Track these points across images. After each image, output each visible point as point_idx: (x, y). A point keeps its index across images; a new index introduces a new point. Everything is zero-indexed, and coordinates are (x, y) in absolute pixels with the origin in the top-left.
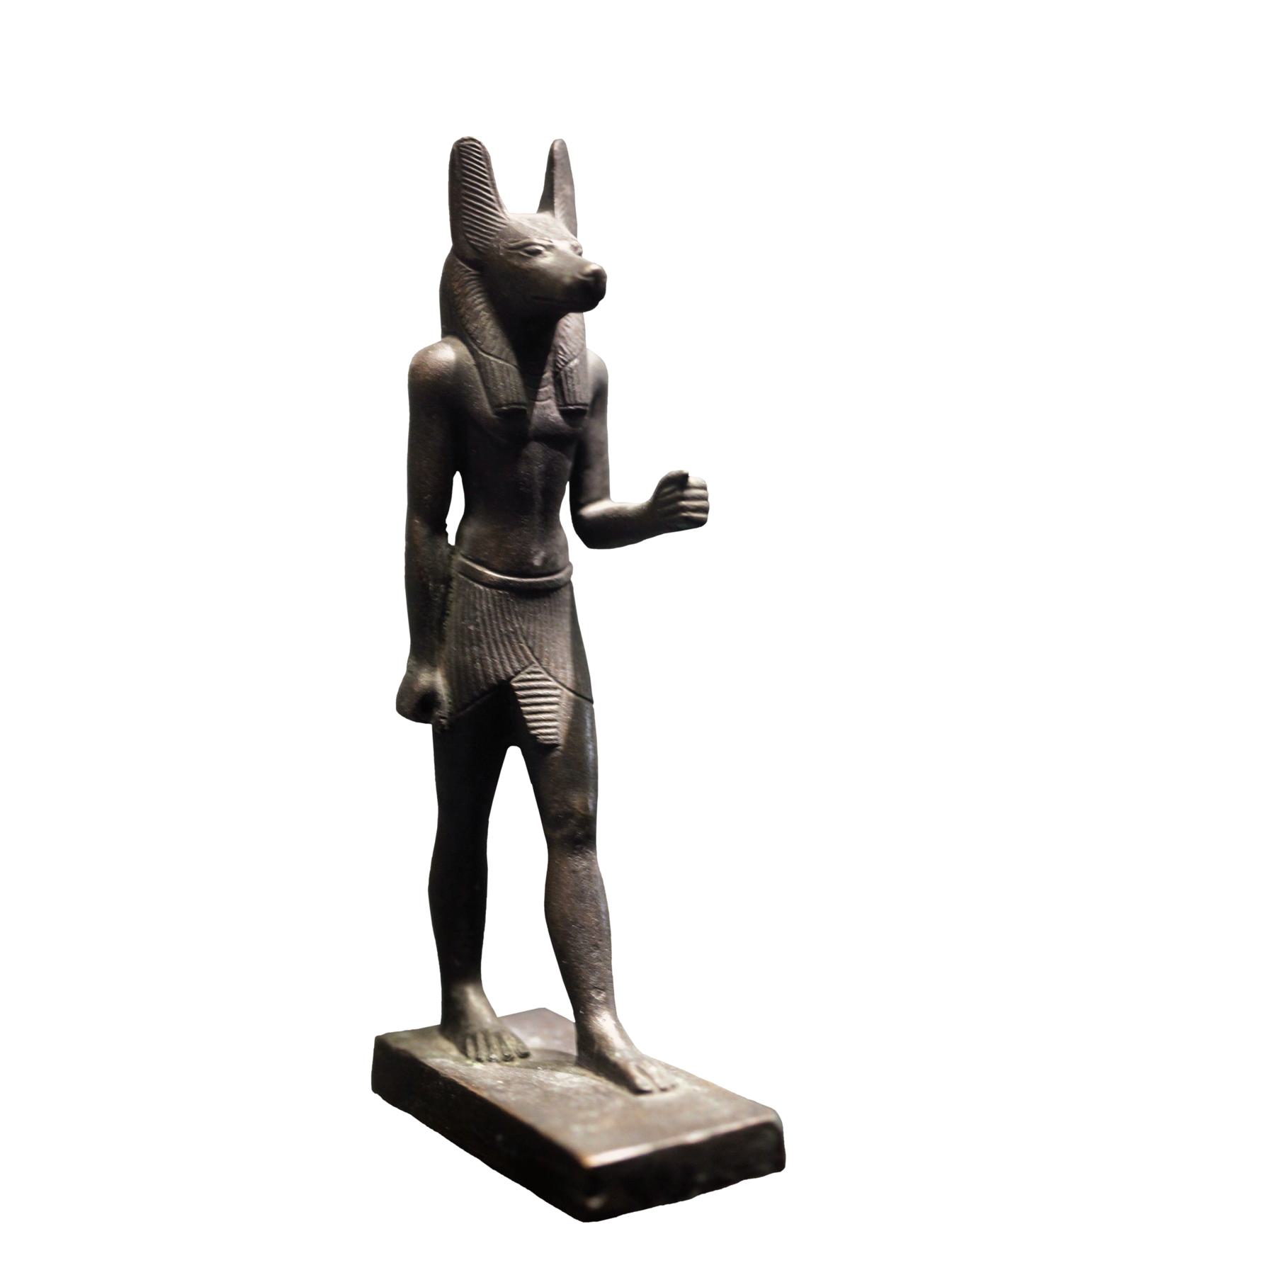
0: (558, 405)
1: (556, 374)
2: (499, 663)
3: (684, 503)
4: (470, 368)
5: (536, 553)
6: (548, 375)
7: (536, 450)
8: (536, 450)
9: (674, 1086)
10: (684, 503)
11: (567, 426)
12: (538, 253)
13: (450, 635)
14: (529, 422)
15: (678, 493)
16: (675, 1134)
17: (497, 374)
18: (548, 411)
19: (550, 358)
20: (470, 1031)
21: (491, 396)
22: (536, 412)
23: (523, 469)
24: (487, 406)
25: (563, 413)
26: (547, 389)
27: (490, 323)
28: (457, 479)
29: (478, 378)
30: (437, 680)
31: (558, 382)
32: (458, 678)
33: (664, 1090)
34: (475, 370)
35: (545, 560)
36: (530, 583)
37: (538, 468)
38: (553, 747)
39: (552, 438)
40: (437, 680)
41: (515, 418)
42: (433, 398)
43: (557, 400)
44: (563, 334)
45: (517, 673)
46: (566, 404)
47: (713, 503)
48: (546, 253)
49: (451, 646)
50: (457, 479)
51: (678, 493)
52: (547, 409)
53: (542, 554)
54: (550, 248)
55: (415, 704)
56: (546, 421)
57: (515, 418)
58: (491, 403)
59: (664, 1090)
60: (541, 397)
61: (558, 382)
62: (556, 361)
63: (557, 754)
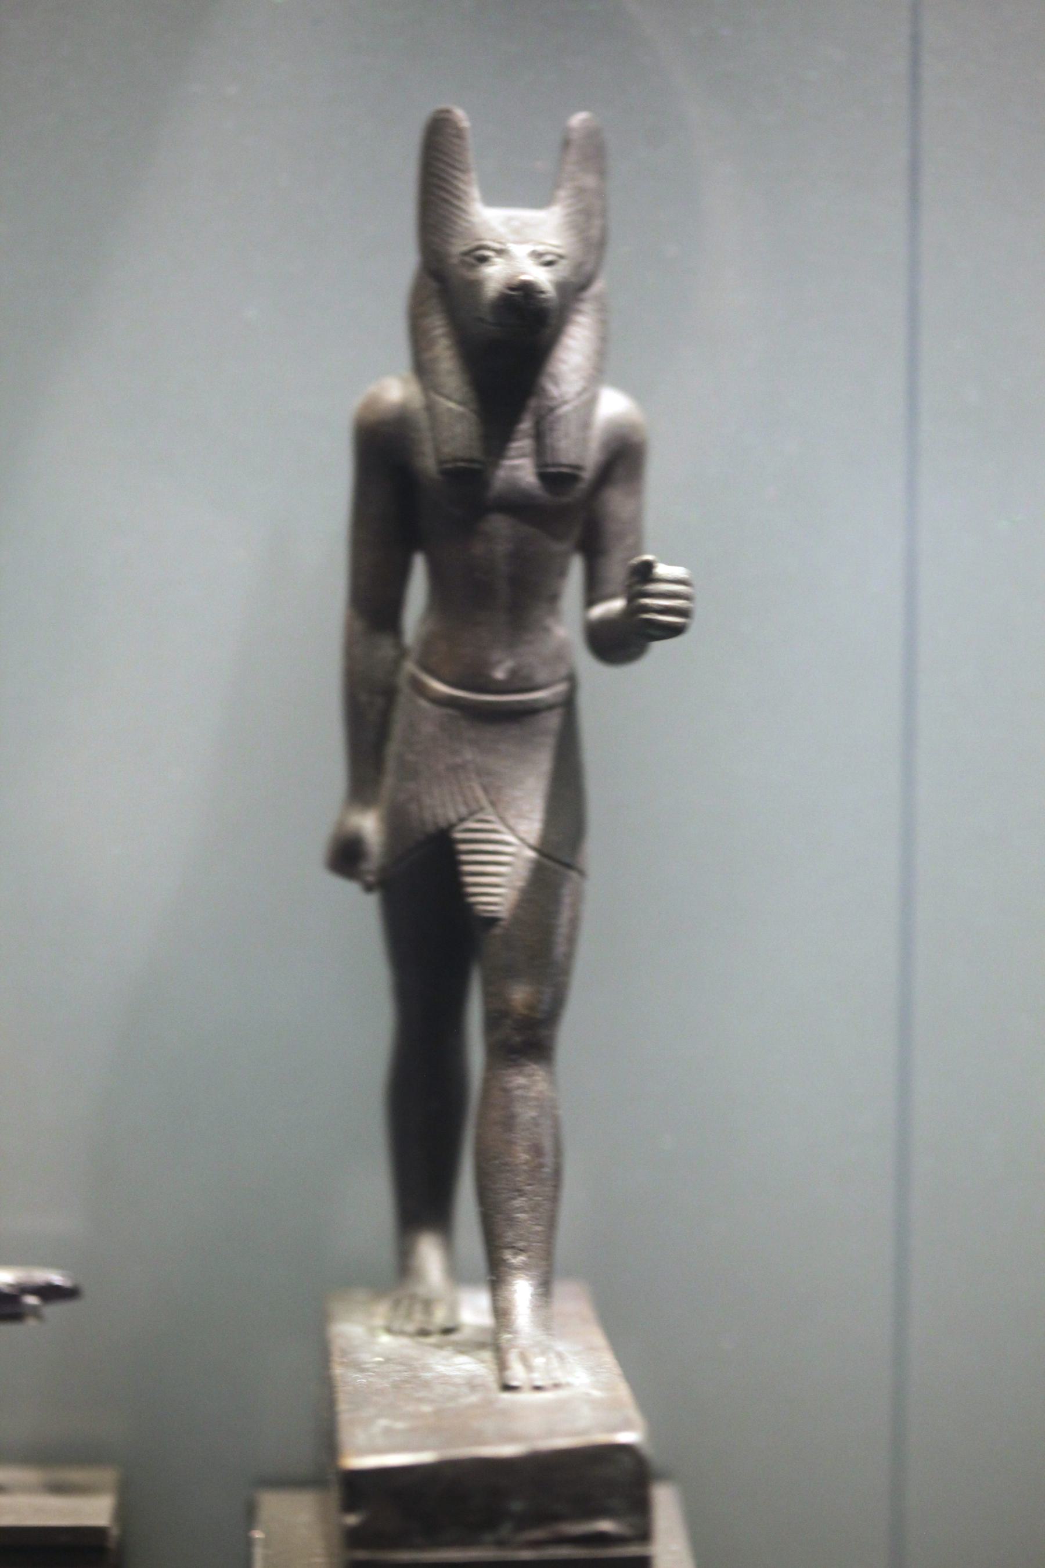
2: (440, 806)
5: (499, 662)
6: (526, 425)
7: (499, 525)
8: (499, 525)
9: (568, 1385)
12: (484, 260)
13: (391, 764)
16: (485, 1443)
20: (421, 1290)
23: (478, 549)
25: (544, 477)
26: (522, 444)
30: (369, 824)
31: (539, 436)
32: (396, 824)
33: (538, 1388)
35: (513, 673)
36: (472, 701)
37: (502, 548)
38: (492, 921)
39: (517, 505)
40: (369, 824)
41: (470, 480)
42: (382, 450)
45: (462, 820)
47: (700, 609)
48: (498, 260)
49: (389, 781)
53: (509, 664)
54: (500, 252)
55: (346, 856)
57: (470, 480)
59: (538, 1388)
60: (512, 453)
61: (539, 436)
63: (497, 931)
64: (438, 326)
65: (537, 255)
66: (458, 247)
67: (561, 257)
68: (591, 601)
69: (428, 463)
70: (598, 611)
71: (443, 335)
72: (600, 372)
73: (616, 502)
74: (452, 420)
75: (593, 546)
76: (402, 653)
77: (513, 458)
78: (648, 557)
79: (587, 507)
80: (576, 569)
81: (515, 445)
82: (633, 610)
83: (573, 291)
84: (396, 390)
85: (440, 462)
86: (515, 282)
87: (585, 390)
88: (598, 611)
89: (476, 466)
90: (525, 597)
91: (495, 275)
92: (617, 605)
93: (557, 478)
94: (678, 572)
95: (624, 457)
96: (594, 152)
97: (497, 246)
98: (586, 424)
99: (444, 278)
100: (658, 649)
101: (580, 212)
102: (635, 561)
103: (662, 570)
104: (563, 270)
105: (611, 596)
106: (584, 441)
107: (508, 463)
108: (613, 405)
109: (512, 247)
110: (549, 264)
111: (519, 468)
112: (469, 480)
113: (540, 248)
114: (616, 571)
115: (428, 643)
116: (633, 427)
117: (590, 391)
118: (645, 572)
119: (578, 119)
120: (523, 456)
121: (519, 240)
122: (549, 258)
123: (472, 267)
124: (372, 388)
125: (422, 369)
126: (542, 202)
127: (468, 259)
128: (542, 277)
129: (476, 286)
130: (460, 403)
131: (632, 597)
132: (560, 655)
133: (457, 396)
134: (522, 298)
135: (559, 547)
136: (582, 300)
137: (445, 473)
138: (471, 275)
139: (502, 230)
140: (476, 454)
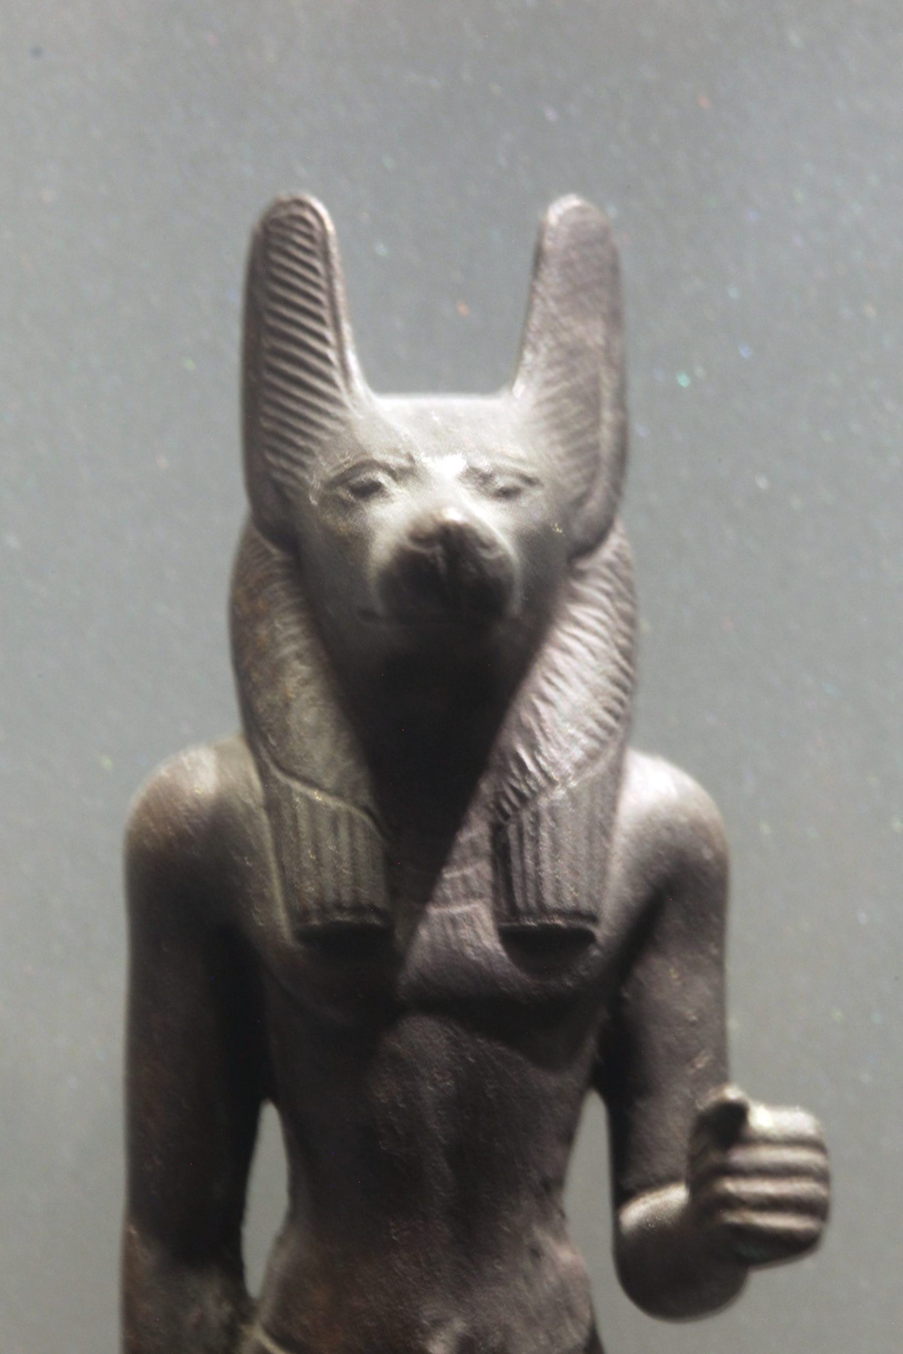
0: (497, 916)
1: (497, 831)
3: (731, 1186)
4: (250, 813)
5: (438, 1323)
6: (475, 832)
7: (425, 1038)
8: (425, 1038)
10: (731, 1186)
11: (521, 975)
12: (372, 490)
14: (398, 959)
15: (714, 1158)
17: (304, 826)
18: (466, 933)
19: (485, 788)
21: (290, 888)
22: (424, 933)
24: (281, 916)
25: (511, 936)
27: (310, 692)
28: (270, 1121)
29: (268, 838)
34: (264, 817)
37: (434, 1088)
39: (463, 999)
41: (360, 950)
42: (183, 889)
43: (496, 900)
44: (527, 717)
46: (514, 911)
47: (843, 1198)
50: (270, 1121)
51: (714, 1158)
52: (464, 921)
53: (459, 1325)
56: (454, 960)
58: (289, 909)
61: (501, 855)
62: (499, 795)
64: (288, 638)
65: (480, 480)
66: (320, 471)
67: (530, 481)
68: (622, 1196)
69: (275, 918)
70: (637, 1212)
71: (298, 656)
72: (623, 724)
73: (669, 982)
74: (321, 832)
75: (625, 1079)
76: (242, 1306)
77: (446, 901)
78: (732, 1093)
79: (606, 998)
80: (594, 1116)
81: (450, 874)
82: (707, 1205)
83: (561, 555)
84: (207, 770)
85: (299, 915)
86: (429, 527)
87: (592, 756)
88: (637, 1212)
89: (375, 921)
90: (483, 1190)
91: (391, 519)
92: (676, 1196)
93: (542, 940)
94: (797, 1121)
95: (682, 892)
96: (599, 277)
97: (394, 461)
98: (601, 826)
99: (294, 540)
100: (764, 1284)
101: (572, 394)
102: (709, 1099)
103: (762, 1118)
104: (535, 507)
105: (669, 1180)
106: (598, 863)
107: (434, 911)
108: (654, 787)
109: (424, 460)
110: (506, 494)
111: (464, 921)
112: (360, 950)
113: (484, 464)
114: (671, 1128)
115: (289, 1291)
116: (697, 827)
117: (607, 758)
118: (729, 1124)
119: (562, 210)
120: (471, 895)
121: (445, 452)
122: (501, 482)
123: (346, 506)
124: (163, 771)
125: (260, 728)
126: (492, 378)
127: (344, 493)
128: (495, 523)
129: (356, 543)
130: (337, 793)
131: (702, 1179)
132: (566, 1302)
133: (329, 782)
134: (445, 561)
135: (551, 1082)
136: (581, 575)
137: (305, 936)
138: (343, 525)
139: (406, 431)
140: (373, 893)
